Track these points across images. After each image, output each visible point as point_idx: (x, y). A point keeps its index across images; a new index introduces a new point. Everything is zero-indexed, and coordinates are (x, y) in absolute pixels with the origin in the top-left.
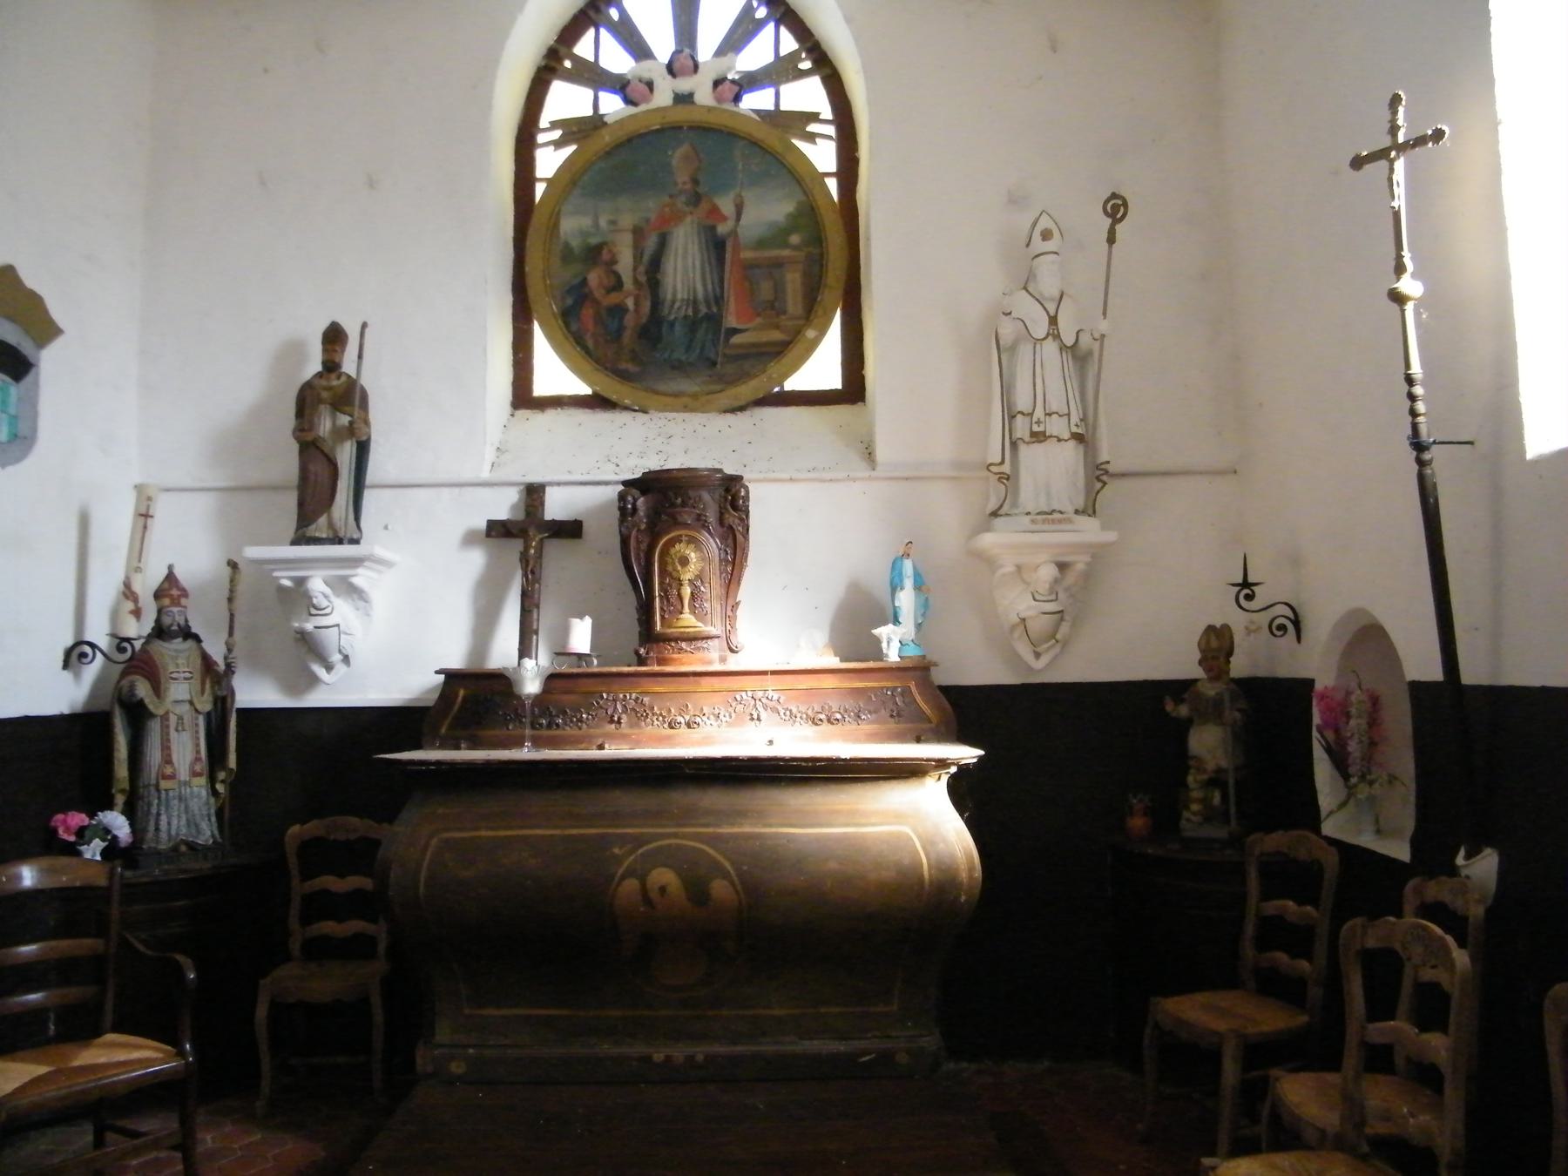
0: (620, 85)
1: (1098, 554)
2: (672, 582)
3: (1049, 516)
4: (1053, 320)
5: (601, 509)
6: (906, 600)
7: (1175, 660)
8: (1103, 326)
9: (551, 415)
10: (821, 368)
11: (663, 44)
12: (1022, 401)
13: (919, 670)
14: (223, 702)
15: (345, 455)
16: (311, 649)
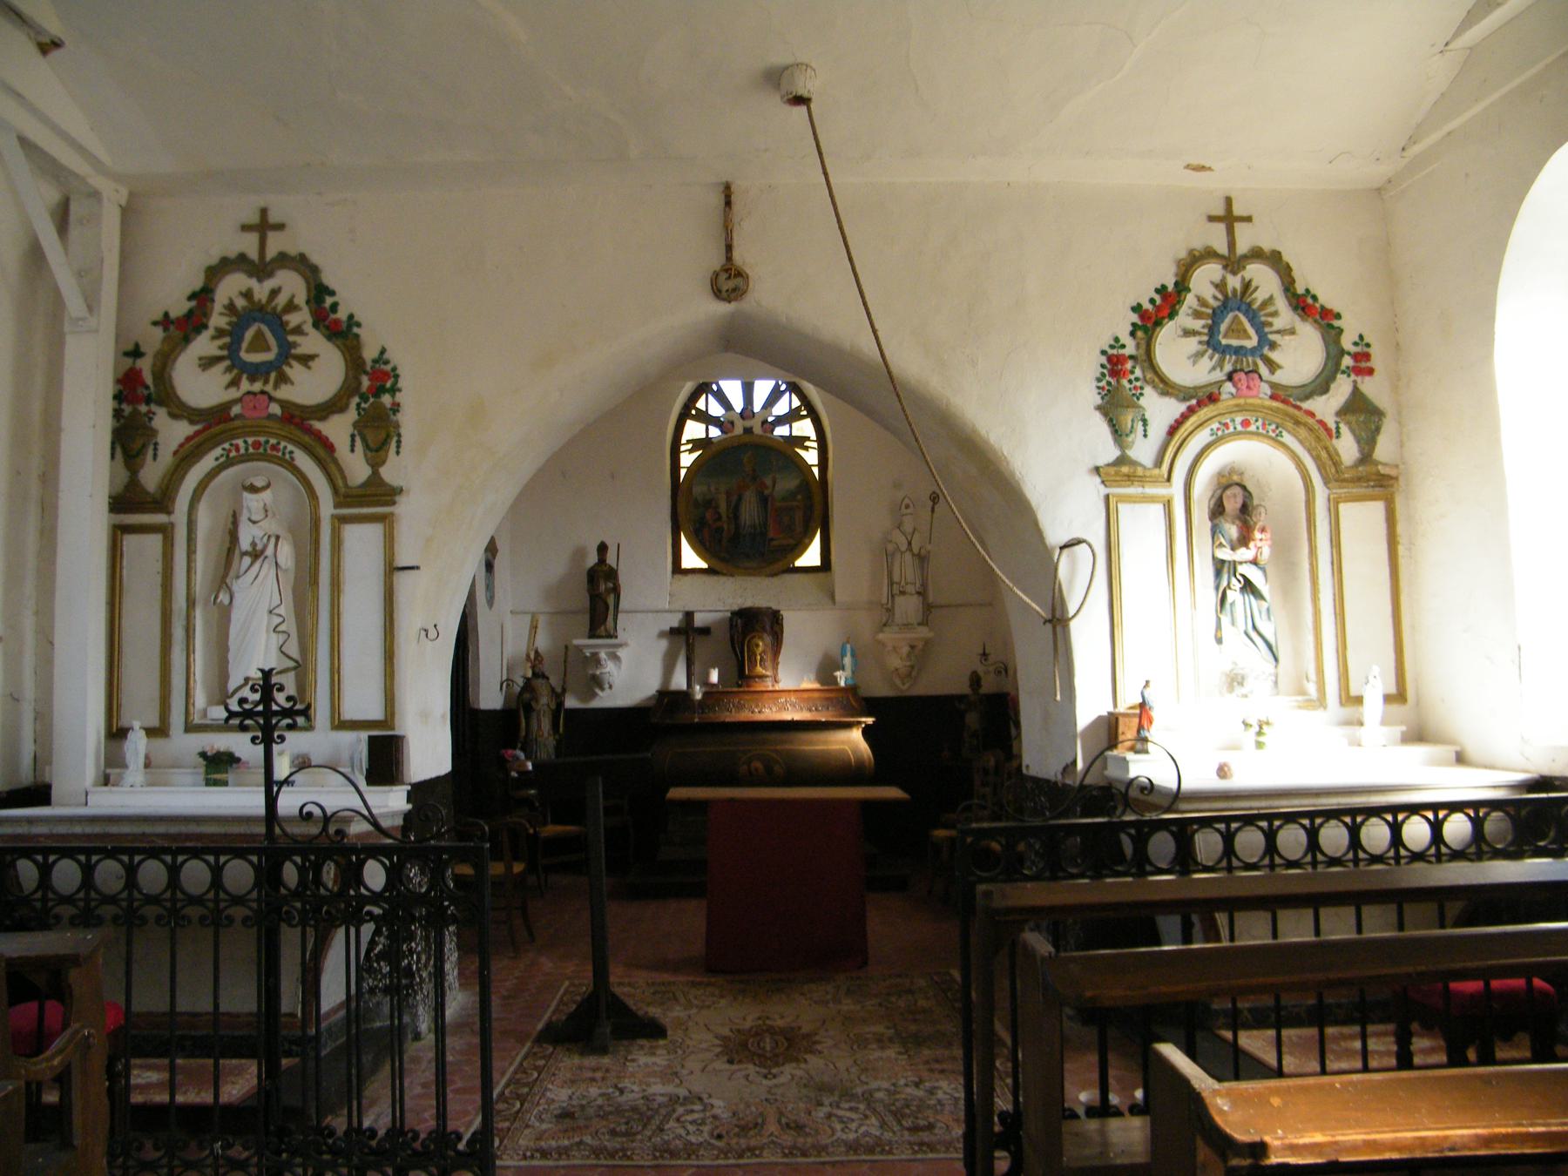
0: (715, 421)
1: (927, 642)
2: (752, 655)
3: (907, 626)
4: (910, 544)
5: (721, 621)
6: (847, 661)
7: (961, 686)
8: (929, 547)
9: (689, 579)
10: (811, 556)
11: (738, 405)
12: (896, 578)
13: (852, 689)
14: (560, 704)
15: (611, 600)
16: (597, 682)
